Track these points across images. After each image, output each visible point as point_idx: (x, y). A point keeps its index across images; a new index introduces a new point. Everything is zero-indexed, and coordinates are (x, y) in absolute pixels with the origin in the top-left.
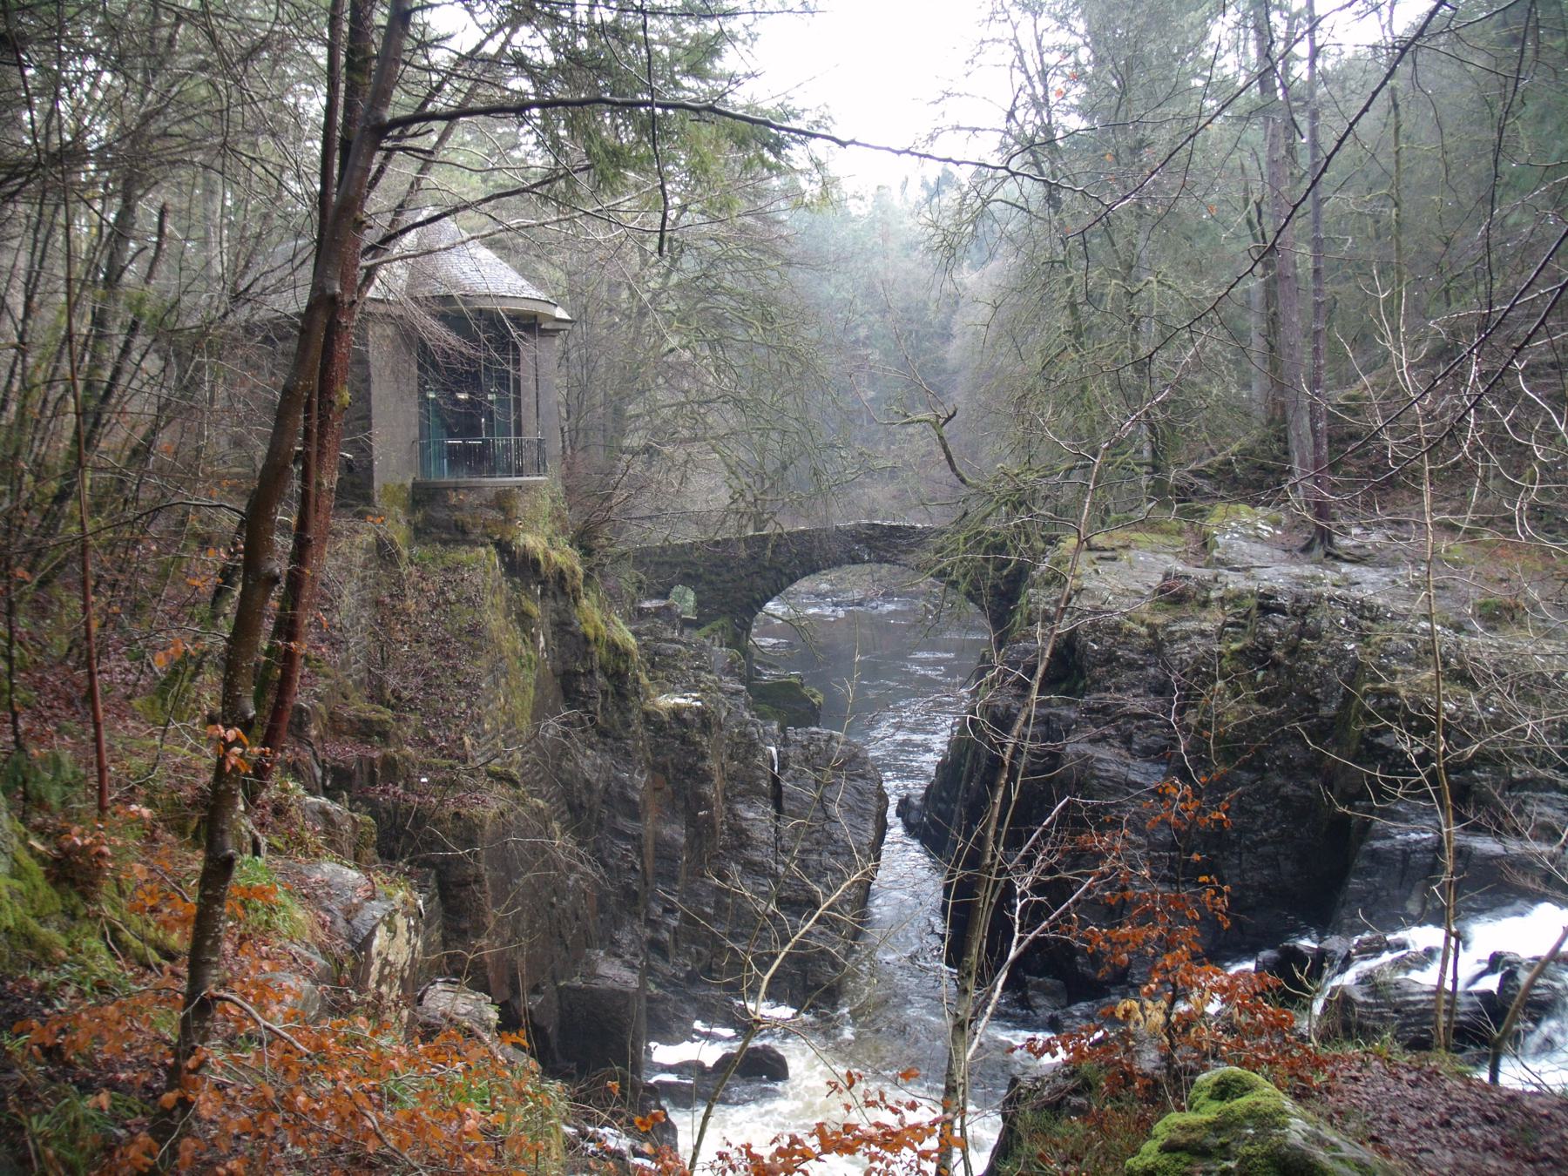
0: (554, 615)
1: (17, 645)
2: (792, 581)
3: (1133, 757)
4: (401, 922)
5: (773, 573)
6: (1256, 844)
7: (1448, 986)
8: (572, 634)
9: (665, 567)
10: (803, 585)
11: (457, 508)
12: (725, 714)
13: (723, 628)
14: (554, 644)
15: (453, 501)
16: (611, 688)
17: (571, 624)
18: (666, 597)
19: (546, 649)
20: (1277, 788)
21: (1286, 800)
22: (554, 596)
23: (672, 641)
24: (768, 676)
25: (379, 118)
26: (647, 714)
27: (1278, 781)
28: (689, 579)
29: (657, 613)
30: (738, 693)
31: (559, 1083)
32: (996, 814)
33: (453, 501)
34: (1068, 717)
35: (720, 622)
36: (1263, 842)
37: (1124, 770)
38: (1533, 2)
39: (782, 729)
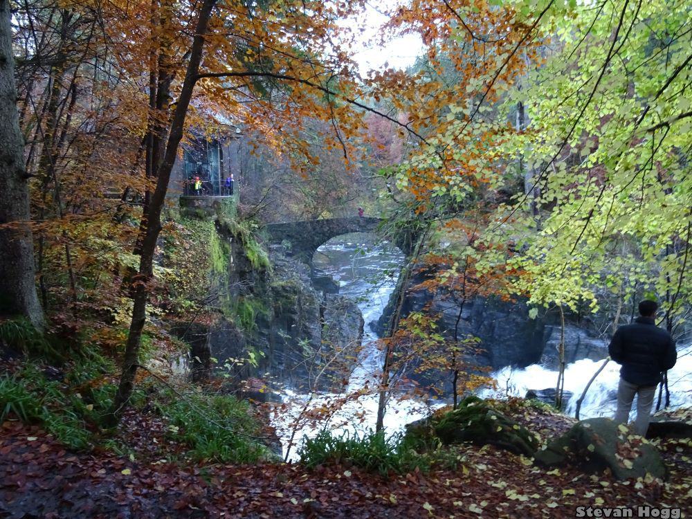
4: (181, 360)
6: (505, 341)
7: (560, 388)
9: (278, 233)
10: (333, 240)
11: (198, 207)
15: (197, 205)
18: (280, 244)
20: (514, 319)
21: (517, 324)
23: (283, 260)
24: (319, 275)
26: (273, 288)
27: (515, 317)
28: (289, 237)
29: (277, 250)
31: (274, 423)
32: (656, 404)
33: (197, 205)
36: (508, 340)
38: (628, 1)
39: (324, 295)
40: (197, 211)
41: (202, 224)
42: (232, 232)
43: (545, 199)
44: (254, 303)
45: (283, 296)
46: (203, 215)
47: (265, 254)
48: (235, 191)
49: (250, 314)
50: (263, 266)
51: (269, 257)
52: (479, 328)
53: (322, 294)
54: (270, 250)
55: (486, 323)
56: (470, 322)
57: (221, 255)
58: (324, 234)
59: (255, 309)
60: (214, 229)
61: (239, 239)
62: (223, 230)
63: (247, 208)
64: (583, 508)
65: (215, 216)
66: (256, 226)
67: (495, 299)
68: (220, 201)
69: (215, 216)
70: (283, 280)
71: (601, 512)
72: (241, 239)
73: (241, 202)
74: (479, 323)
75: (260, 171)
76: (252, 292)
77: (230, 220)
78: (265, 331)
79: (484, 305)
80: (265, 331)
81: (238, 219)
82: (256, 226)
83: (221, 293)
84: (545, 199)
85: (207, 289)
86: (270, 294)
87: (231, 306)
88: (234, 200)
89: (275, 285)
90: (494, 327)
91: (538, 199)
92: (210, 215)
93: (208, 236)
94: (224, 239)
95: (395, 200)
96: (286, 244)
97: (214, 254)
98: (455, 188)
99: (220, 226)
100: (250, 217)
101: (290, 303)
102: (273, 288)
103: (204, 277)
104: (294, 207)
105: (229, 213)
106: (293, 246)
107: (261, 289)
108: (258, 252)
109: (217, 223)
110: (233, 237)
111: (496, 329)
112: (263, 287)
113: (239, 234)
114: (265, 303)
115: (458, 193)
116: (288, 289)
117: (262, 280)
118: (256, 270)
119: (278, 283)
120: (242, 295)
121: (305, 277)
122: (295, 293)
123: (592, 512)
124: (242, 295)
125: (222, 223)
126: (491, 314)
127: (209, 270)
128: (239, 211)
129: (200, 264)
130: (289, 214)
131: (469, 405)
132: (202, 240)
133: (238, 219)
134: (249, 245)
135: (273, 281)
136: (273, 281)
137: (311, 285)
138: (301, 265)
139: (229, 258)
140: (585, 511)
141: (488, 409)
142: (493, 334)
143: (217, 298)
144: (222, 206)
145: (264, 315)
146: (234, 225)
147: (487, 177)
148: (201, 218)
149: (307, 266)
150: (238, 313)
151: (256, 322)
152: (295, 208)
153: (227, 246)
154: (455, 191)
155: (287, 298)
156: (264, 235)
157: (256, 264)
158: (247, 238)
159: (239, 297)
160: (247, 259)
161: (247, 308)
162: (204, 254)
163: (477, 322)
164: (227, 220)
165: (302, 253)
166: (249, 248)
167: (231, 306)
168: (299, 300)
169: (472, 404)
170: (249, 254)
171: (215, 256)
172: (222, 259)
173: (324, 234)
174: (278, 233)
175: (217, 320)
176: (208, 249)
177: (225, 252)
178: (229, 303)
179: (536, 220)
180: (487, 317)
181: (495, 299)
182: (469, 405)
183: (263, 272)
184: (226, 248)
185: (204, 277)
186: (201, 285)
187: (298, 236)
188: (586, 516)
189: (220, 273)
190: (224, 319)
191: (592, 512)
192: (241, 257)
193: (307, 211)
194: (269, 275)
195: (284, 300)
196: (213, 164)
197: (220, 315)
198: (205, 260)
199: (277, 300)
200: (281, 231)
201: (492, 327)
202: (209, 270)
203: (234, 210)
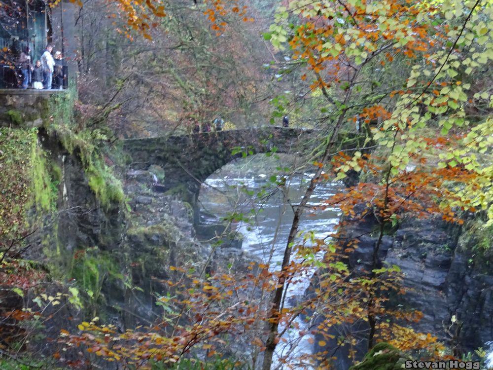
0: (73, 175)
1: (93, 332)
2: (224, 163)
3: (427, 267)
5: (213, 157)
8: (83, 186)
9: (145, 153)
10: (229, 167)
11: (12, 107)
12: (178, 239)
13: (181, 191)
14: (72, 192)
15: (10, 103)
16: (107, 220)
17: (83, 180)
19: (68, 195)
22: (73, 163)
23: (147, 194)
25: (454, 314)
26: (130, 238)
28: (160, 160)
29: (139, 179)
30: (186, 228)
33: (10, 103)
34: (387, 243)
35: (179, 188)
37: (421, 274)
40: (11, 112)
41: (18, 133)
42: (66, 145)
43: (476, 60)
44: (100, 260)
45: (146, 251)
46: (19, 120)
47: (118, 184)
48: (70, 82)
49: (93, 278)
50: (115, 201)
51: (125, 189)
52: (460, 301)
53: (210, 249)
54: (127, 179)
55: (470, 292)
56: (446, 292)
57: (47, 182)
58: (217, 156)
59: (101, 270)
60: (37, 141)
61: (77, 157)
62: (52, 143)
63: (89, 109)
64: (411, 362)
65: (38, 121)
66: (105, 137)
67: (484, 254)
68: (47, 97)
69: (38, 121)
70: (147, 225)
71: (423, 364)
72: (79, 158)
73: (81, 99)
74: (461, 293)
75: (114, 52)
76: (97, 242)
77: (62, 127)
78: (118, 306)
79: (467, 264)
80: (118, 306)
81: (75, 126)
82: (105, 137)
83: (45, 242)
84: (476, 60)
85: (25, 235)
86: (125, 246)
87: (63, 264)
88: (69, 96)
89: (133, 232)
90: (484, 299)
91: (466, 62)
92: (31, 118)
93: (27, 151)
94: (53, 157)
95: (325, 94)
96: (157, 174)
97: (36, 181)
98: (353, 46)
99: (46, 136)
100: (95, 123)
101: (159, 261)
102: (131, 238)
103: (19, 217)
104: (166, 115)
105: (61, 116)
106: (167, 175)
107: (110, 238)
108: (106, 179)
109: (42, 131)
110: (67, 154)
111: (486, 302)
112: (114, 234)
113: (77, 150)
114: (117, 261)
115: (357, 52)
116: (154, 238)
117: (113, 223)
118: (104, 207)
119: (138, 229)
120: (80, 248)
121: (184, 222)
122: (166, 245)
123: (417, 365)
124: (80, 248)
125: (50, 131)
126: (478, 279)
127: (28, 205)
128: (76, 115)
129: (14, 195)
130: (161, 123)
131: (376, 354)
132: (18, 158)
133: (75, 126)
134: (92, 168)
135: (131, 226)
136: (131, 226)
137: (193, 235)
138: (178, 203)
139: (59, 187)
140: (412, 364)
141: (399, 356)
142: (481, 311)
143: (41, 250)
144: (50, 105)
145: (115, 280)
146: (68, 137)
147: (392, 28)
148: (16, 124)
149: (187, 204)
150: (73, 276)
151: (102, 291)
152: (171, 115)
153: (57, 168)
154: (352, 50)
155: (153, 253)
156: (120, 156)
157: (104, 198)
158: (90, 157)
159: (76, 251)
160: (90, 191)
161: (89, 268)
162: (21, 180)
163: (456, 291)
164: (58, 127)
165: (182, 186)
166: (92, 173)
167: (63, 264)
168: (172, 257)
169: (380, 352)
170: (92, 182)
171: (38, 184)
172: (49, 189)
173: (217, 156)
174: (145, 153)
175: (39, 282)
176: (27, 173)
177: (54, 178)
178: (60, 258)
179: (465, 91)
180: (473, 283)
181: (484, 254)
182: (376, 354)
183: (114, 212)
184: (56, 173)
185: (19, 217)
186: (15, 228)
187: (176, 159)
188: (413, 367)
189: (45, 211)
190: (49, 280)
191: (417, 365)
192: (82, 192)
193: (188, 117)
194: (124, 216)
195: (148, 257)
196: (37, 39)
197: (41, 273)
198: (22, 189)
199: (137, 257)
200: (148, 151)
201: (479, 301)
202: (28, 205)
203: (69, 113)
